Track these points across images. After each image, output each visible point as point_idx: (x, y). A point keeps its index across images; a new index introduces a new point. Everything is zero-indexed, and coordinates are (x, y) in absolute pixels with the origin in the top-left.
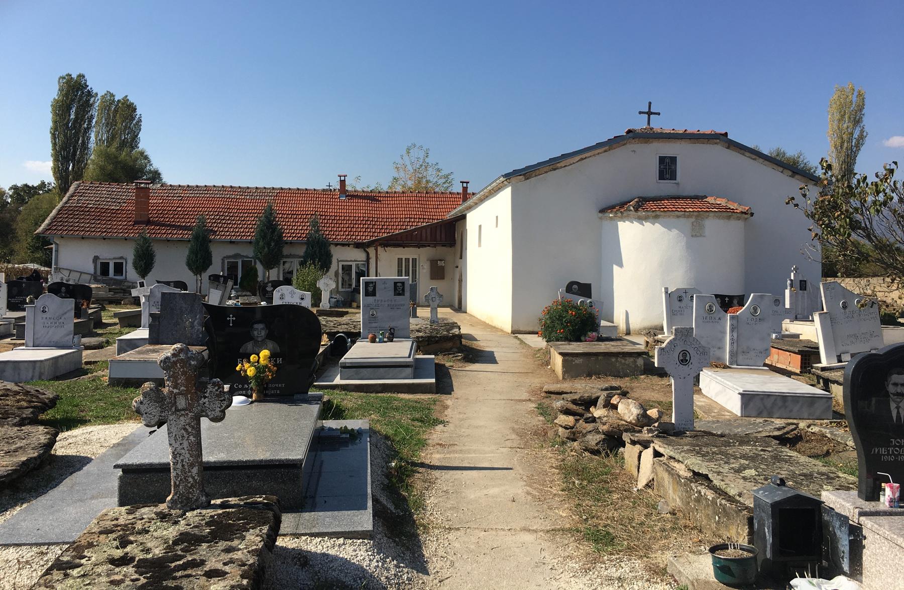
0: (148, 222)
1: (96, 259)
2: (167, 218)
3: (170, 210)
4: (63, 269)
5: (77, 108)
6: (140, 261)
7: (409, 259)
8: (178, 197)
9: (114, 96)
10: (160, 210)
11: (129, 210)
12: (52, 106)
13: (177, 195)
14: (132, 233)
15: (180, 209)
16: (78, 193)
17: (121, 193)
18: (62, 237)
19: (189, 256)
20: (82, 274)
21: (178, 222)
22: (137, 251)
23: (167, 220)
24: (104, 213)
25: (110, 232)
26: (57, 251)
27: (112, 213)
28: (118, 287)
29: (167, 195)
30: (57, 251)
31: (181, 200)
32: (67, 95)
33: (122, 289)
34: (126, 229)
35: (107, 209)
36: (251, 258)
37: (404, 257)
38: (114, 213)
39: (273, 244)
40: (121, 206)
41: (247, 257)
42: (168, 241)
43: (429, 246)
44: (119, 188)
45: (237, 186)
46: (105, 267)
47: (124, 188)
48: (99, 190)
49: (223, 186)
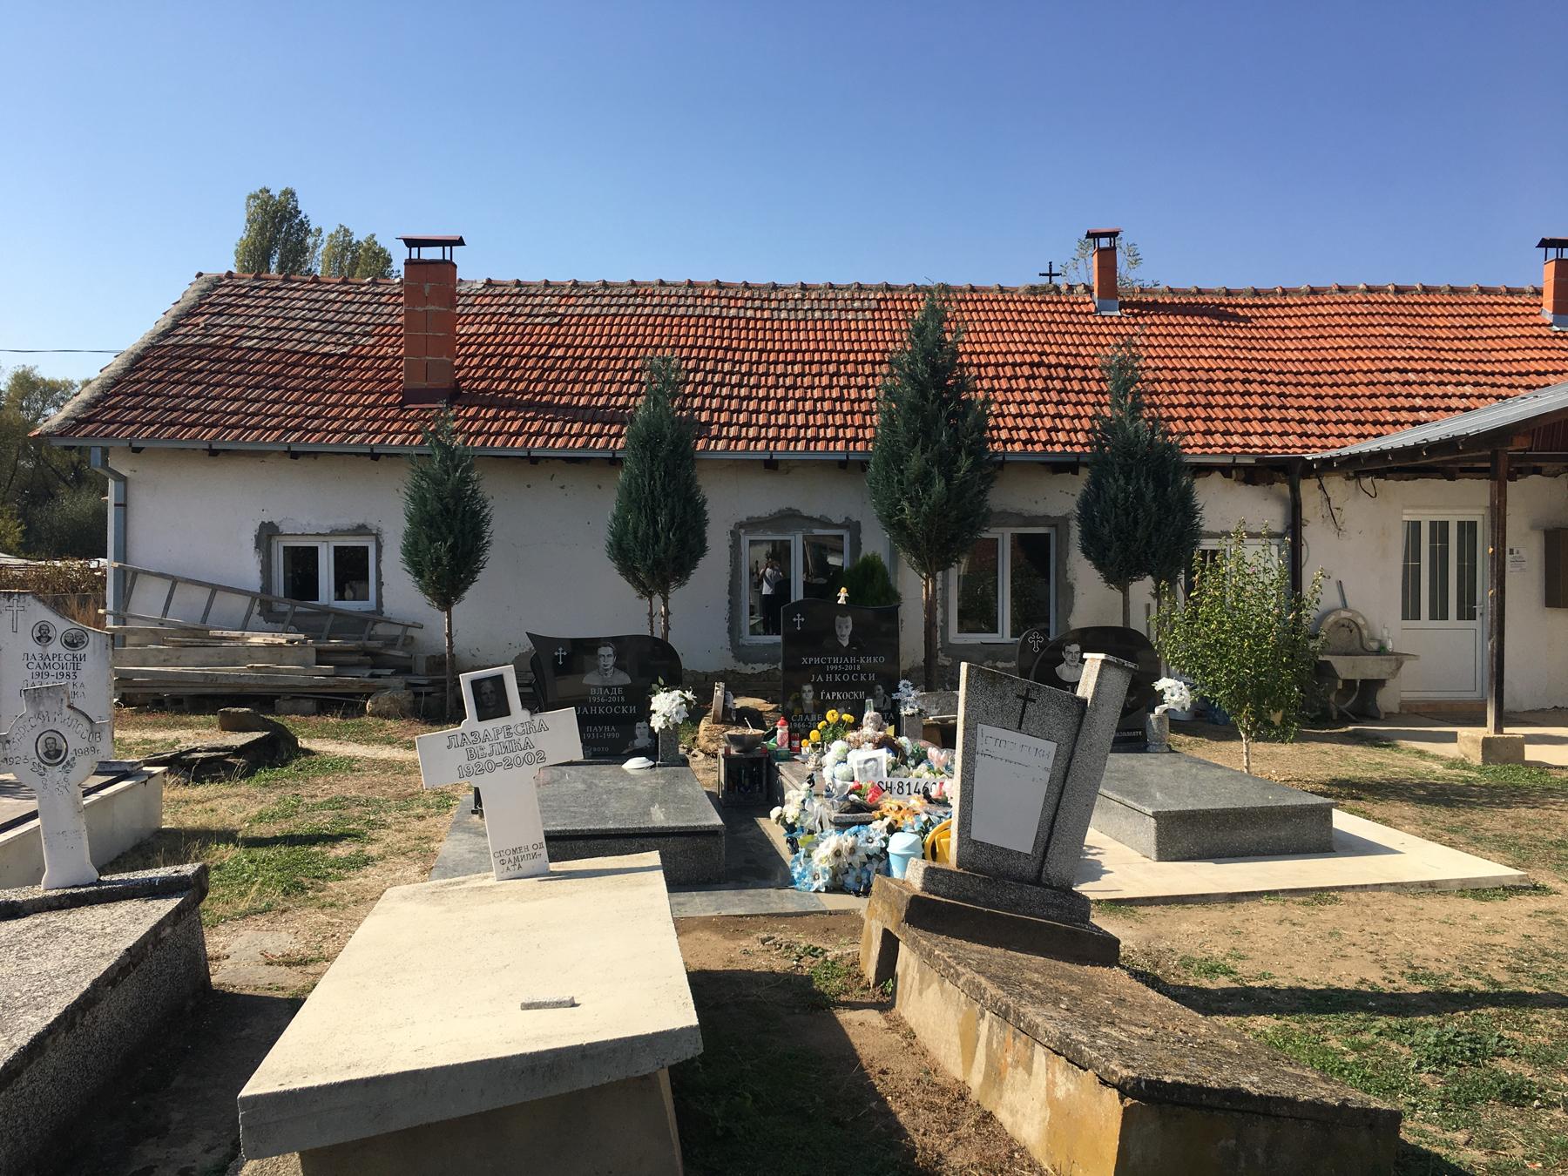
0: (455, 396)
1: (267, 534)
2: (520, 380)
3: (528, 357)
4: (148, 573)
5: (282, 255)
6: (432, 541)
7: (1445, 525)
8: (546, 316)
9: (352, 234)
10: (492, 356)
11: (384, 358)
12: (237, 252)
13: (544, 310)
14: (397, 432)
15: (560, 352)
16: (211, 305)
17: (353, 308)
18: (137, 450)
19: (620, 520)
20: (219, 595)
21: (562, 394)
22: (418, 498)
23: (522, 386)
24: (295, 365)
25: (316, 430)
26: (122, 505)
27: (325, 367)
28: (352, 645)
29: (510, 309)
30: (122, 505)
31: (559, 324)
32: (262, 228)
33: (367, 652)
34: (374, 419)
35: (306, 353)
36: (838, 526)
37: (1426, 518)
38: (331, 368)
39: (99, 573)
40: (355, 345)
41: (825, 523)
42: (534, 461)
43: (1537, 471)
44: (347, 293)
45: (739, 281)
46: (302, 563)
47: (365, 293)
48: (282, 299)
49: (691, 284)
